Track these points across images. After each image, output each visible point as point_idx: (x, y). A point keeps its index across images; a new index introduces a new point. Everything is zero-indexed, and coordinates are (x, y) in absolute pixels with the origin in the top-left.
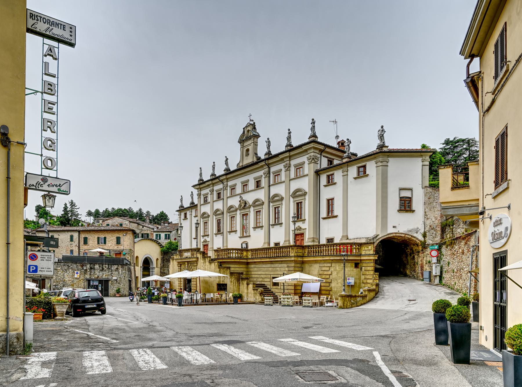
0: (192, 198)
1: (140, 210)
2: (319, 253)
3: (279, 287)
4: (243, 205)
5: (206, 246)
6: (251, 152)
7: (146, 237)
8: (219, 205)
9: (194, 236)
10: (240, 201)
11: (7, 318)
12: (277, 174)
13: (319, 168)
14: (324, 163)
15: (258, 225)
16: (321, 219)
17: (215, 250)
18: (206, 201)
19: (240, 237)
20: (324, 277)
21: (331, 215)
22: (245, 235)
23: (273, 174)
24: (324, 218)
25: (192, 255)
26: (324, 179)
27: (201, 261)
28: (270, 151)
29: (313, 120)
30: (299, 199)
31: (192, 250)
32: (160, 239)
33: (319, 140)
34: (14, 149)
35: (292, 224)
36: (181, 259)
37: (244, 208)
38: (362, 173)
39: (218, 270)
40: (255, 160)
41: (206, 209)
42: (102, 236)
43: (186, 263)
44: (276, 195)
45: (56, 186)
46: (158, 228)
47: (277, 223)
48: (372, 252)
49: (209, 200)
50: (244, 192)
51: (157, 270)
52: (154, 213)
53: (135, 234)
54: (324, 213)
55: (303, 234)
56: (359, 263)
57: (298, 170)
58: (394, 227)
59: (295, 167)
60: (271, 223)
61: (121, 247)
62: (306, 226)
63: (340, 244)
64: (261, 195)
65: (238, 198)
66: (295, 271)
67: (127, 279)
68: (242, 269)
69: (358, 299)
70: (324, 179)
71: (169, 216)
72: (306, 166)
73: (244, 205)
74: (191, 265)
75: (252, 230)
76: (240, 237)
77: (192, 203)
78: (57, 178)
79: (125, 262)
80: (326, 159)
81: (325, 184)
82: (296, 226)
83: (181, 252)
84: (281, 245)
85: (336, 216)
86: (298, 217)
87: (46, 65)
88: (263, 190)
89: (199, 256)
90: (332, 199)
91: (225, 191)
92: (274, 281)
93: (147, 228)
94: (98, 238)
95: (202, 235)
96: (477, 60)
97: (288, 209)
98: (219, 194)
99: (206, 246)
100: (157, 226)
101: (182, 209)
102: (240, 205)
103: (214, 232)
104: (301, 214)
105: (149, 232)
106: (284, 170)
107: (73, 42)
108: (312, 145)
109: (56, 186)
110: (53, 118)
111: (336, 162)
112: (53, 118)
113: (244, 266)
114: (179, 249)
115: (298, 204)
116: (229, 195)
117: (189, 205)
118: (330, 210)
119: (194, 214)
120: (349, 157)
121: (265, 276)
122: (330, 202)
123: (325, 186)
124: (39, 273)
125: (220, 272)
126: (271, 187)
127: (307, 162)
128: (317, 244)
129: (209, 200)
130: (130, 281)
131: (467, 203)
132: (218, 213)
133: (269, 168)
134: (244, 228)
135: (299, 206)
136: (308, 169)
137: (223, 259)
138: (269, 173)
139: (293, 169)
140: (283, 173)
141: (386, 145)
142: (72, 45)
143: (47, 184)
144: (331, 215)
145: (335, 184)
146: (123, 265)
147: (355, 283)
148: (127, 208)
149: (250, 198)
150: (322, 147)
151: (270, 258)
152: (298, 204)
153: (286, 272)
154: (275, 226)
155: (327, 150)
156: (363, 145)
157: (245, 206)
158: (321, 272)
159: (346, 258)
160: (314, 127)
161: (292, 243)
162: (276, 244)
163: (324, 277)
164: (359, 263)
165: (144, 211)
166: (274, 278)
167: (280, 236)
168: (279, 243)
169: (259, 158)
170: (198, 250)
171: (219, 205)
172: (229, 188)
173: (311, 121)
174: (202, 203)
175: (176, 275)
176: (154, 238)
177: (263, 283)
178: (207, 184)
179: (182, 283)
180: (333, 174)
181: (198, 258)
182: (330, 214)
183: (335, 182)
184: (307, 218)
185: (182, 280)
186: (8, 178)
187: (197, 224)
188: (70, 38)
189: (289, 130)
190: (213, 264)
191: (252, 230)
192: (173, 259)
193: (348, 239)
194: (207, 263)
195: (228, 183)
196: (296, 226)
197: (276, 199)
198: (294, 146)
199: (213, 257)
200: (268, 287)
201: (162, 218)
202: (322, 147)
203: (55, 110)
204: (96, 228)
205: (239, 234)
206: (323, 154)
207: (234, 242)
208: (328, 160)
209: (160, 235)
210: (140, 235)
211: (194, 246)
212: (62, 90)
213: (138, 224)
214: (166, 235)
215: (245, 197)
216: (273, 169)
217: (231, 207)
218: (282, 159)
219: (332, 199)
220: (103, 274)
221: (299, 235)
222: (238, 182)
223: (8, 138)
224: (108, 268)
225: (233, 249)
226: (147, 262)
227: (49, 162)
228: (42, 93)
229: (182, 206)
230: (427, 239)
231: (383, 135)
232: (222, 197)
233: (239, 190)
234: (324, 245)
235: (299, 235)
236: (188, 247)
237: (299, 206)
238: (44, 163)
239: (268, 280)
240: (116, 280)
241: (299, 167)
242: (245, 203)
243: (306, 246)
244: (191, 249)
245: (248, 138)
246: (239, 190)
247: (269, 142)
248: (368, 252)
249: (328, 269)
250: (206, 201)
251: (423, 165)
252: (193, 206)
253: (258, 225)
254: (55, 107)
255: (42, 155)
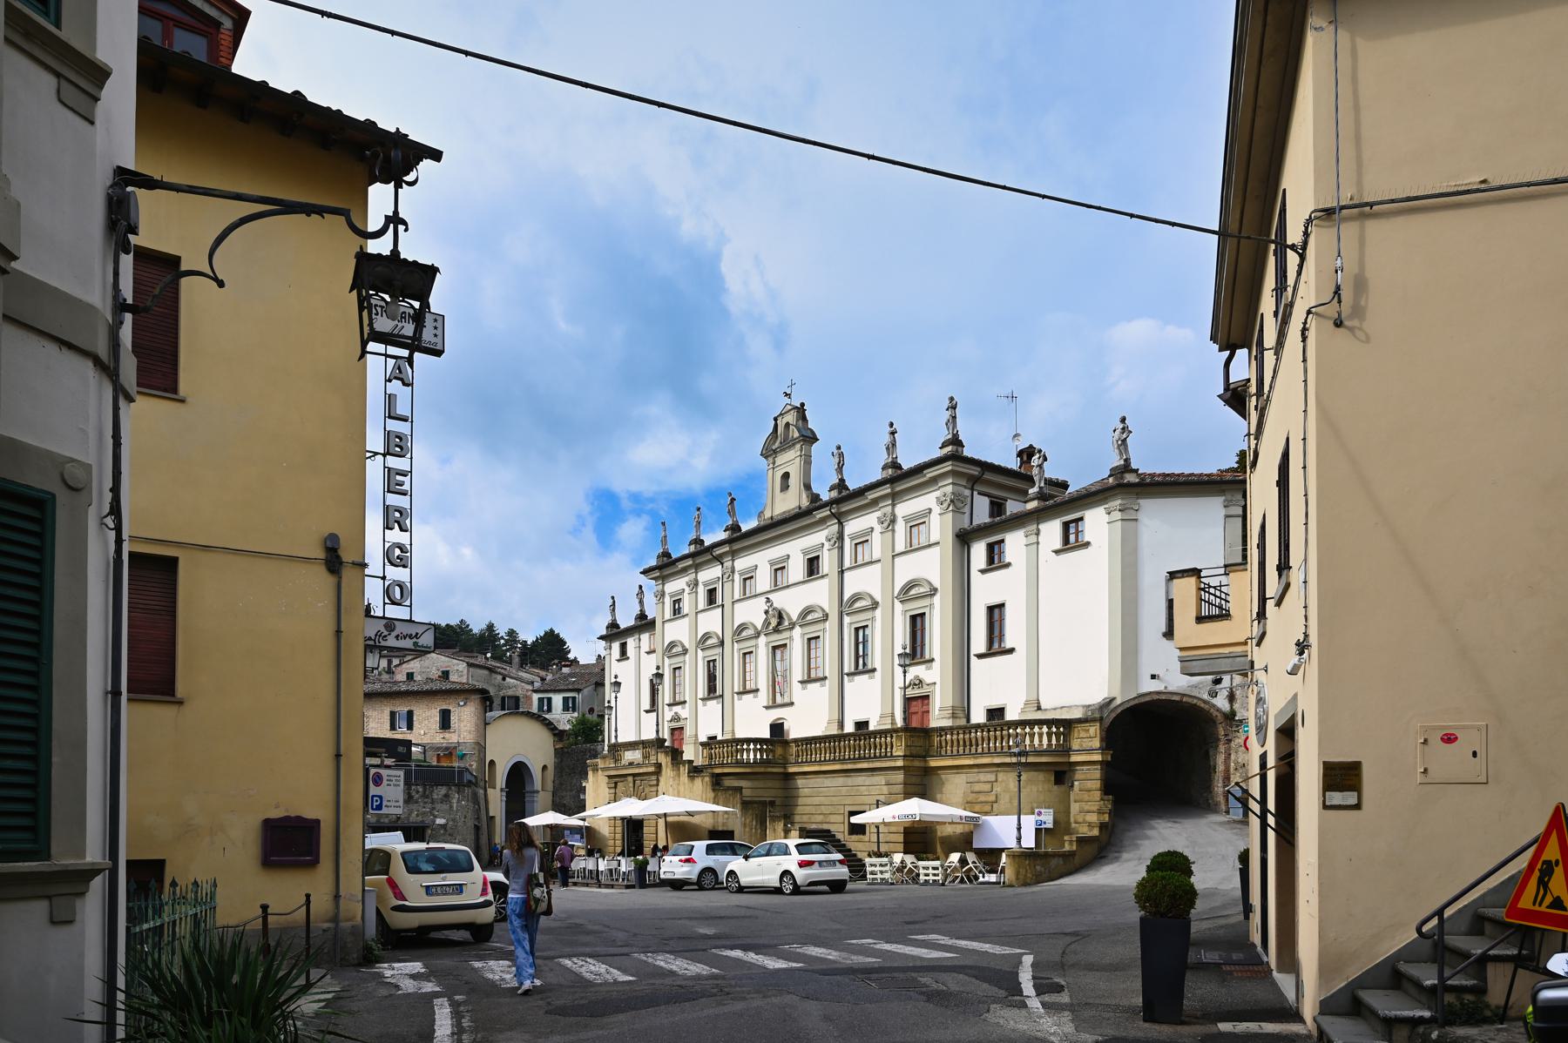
0: (641, 602)
1: (491, 627)
2: (969, 747)
3: (866, 838)
4: (774, 622)
5: (677, 732)
6: (794, 481)
7: (513, 706)
8: (711, 622)
9: (646, 705)
10: (766, 612)
11: (337, 897)
12: (862, 540)
13: (966, 525)
14: (982, 514)
15: (813, 675)
16: (974, 659)
17: (702, 744)
18: (677, 612)
19: (767, 708)
20: (977, 808)
21: (996, 647)
22: (779, 700)
23: (852, 539)
24: (980, 656)
25: (645, 757)
26: (979, 551)
27: (667, 772)
28: (842, 480)
29: (952, 399)
30: (916, 607)
31: (643, 744)
32: (550, 710)
33: (967, 452)
34: (348, 574)
35: (899, 671)
36: (616, 768)
37: (776, 630)
38: (1071, 542)
39: (712, 795)
40: (805, 503)
41: (677, 631)
42: (402, 709)
43: (630, 779)
44: (856, 597)
45: (411, 637)
46: (543, 679)
47: (863, 668)
48: (1096, 743)
49: (686, 607)
50: (777, 588)
51: (544, 797)
52: (529, 635)
53: (486, 700)
54: (979, 643)
55: (927, 697)
56: (1064, 772)
57: (915, 530)
58: (1153, 677)
59: (907, 522)
60: (846, 670)
61: (452, 738)
62: (936, 676)
63: (1023, 723)
64: (820, 594)
65: (760, 605)
66: (908, 795)
67: (471, 823)
68: (773, 793)
69: (1054, 862)
70: (979, 551)
71: (569, 644)
72: (935, 519)
73: (778, 621)
74: (641, 782)
75: (796, 687)
76: (767, 708)
77: (642, 616)
78: (410, 621)
79: (467, 777)
80: (986, 500)
81: (983, 566)
82: (909, 677)
83: (616, 748)
84: (872, 728)
85: (1011, 651)
86: (915, 652)
87: (390, 399)
88: (825, 581)
89: (664, 759)
90: (1002, 606)
91: (728, 586)
92: (855, 820)
93: (521, 682)
94: (393, 714)
95: (667, 701)
96: (1242, 354)
97: (888, 635)
98: (711, 593)
99: (677, 732)
100: (543, 673)
101: (614, 633)
102: (767, 623)
103: (700, 695)
104: (923, 645)
105: (519, 693)
106: (878, 529)
107: (439, 347)
108: (947, 467)
109: (411, 637)
110: (402, 501)
111: (1012, 507)
112: (402, 501)
113: (777, 784)
114: (609, 738)
115: (913, 618)
116: (737, 597)
117: (631, 623)
118: (996, 633)
119: (645, 646)
120: (1041, 496)
121: (831, 809)
122: (995, 613)
123: (983, 571)
124: (384, 811)
125: (716, 802)
126: (846, 575)
127: (937, 510)
128: (963, 722)
129: (686, 610)
130: (477, 828)
131: (1226, 650)
132: (709, 642)
133: (840, 523)
134: (777, 683)
135: (917, 623)
136: (940, 527)
137: (722, 765)
138: (841, 537)
139: (900, 527)
140: (876, 538)
141: (1134, 466)
142: (438, 353)
143: (394, 634)
144: (996, 647)
145: (1008, 565)
146: (460, 786)
147: (1055, 822)
148: (454, 622)
149: (792, 602)
150: (975, 471)
151: (842, 761)
152: (913, 618)
153: (882, 798)
154: (857, 678)
155: (988, 476)
156: (1078, 466)
157: (779, 624)
158: (971, 797)
159: (1023, 760)
160: (954, 418)
161: (899, 723)
162: (862, 725)
163: (977, 808)
164: (1064, 772)
165: (502, 631)
166: (853, 813)
167: (872, 702)
168: (866, 723)
169: (815, 498)
170: (659, 743)
171: (711, 622)
172: (737, 577)
173: (947, 403)
174: (667, 616)
175: (604, 809)
176: (535, 709)
177: (825, 827)
178: (681, 565)
179: (619, 830)
180: (1003, 541)
181: (659, 766)
182: (996, 646)
183: (1007, 560)
184: (936, 655)
185: (619, 823)
186: (338, 632)
187: (659, 676)
188: (433, 340)
189: (891, 425)
190: (698, 782)
191: (796, 687)
192: (595, 770)
193: (1039, 708)
194: (684, 778)
195: (737, 563)
196: (909, 677)
197: (858, 605)
198: (905, 467)
199: (699, 762)
200: (839, 836)
201: (551, 649)
202: (975, 471)
203: (406, 487)
204: (386, 688)
205: (763, 697)
206: (978, 487)
207: (752, 721)
208: (992, 503)
209: (549, 700)
210: (497, 702)
211: (649, 734)
212: (419, 450)
213: (492, 670)
214: (565, 700)
215: (779, 600)
216: (853, 526)
217: (743, 627)
218: (875, 502)
219: (1002, 606)
220: (411, 812)
221: (916, 702)
222: (759, 560)
223: (338, 557)
224: (424, 796)
225: (748, 741)
226: (519, 773)
227: (397, 589)
228: (384, 455)
229: (613, 625)
230: (1236, 706)
231: (1124, 441)
232: (719, 602)
233: (763, 581)
234: (978, 726)
235: (916, 702)
236: (632, 738)
237: (917, 623)
238: (387, 592)
239: (839, 818)
240: (443, 826)
241: (917, 522)
242: (780, 616)
243: (934, 729)
244: (643, 742)
245: (787, 444)
246: (763, 581)
247: (841, 455)
248: (1088, 744)
249: (987, 787)
250: (677, 612)
251: (1227, 516)
252: (644, 624)
253: (813, 675)
254: (407, 480)
255: (384, 578)
